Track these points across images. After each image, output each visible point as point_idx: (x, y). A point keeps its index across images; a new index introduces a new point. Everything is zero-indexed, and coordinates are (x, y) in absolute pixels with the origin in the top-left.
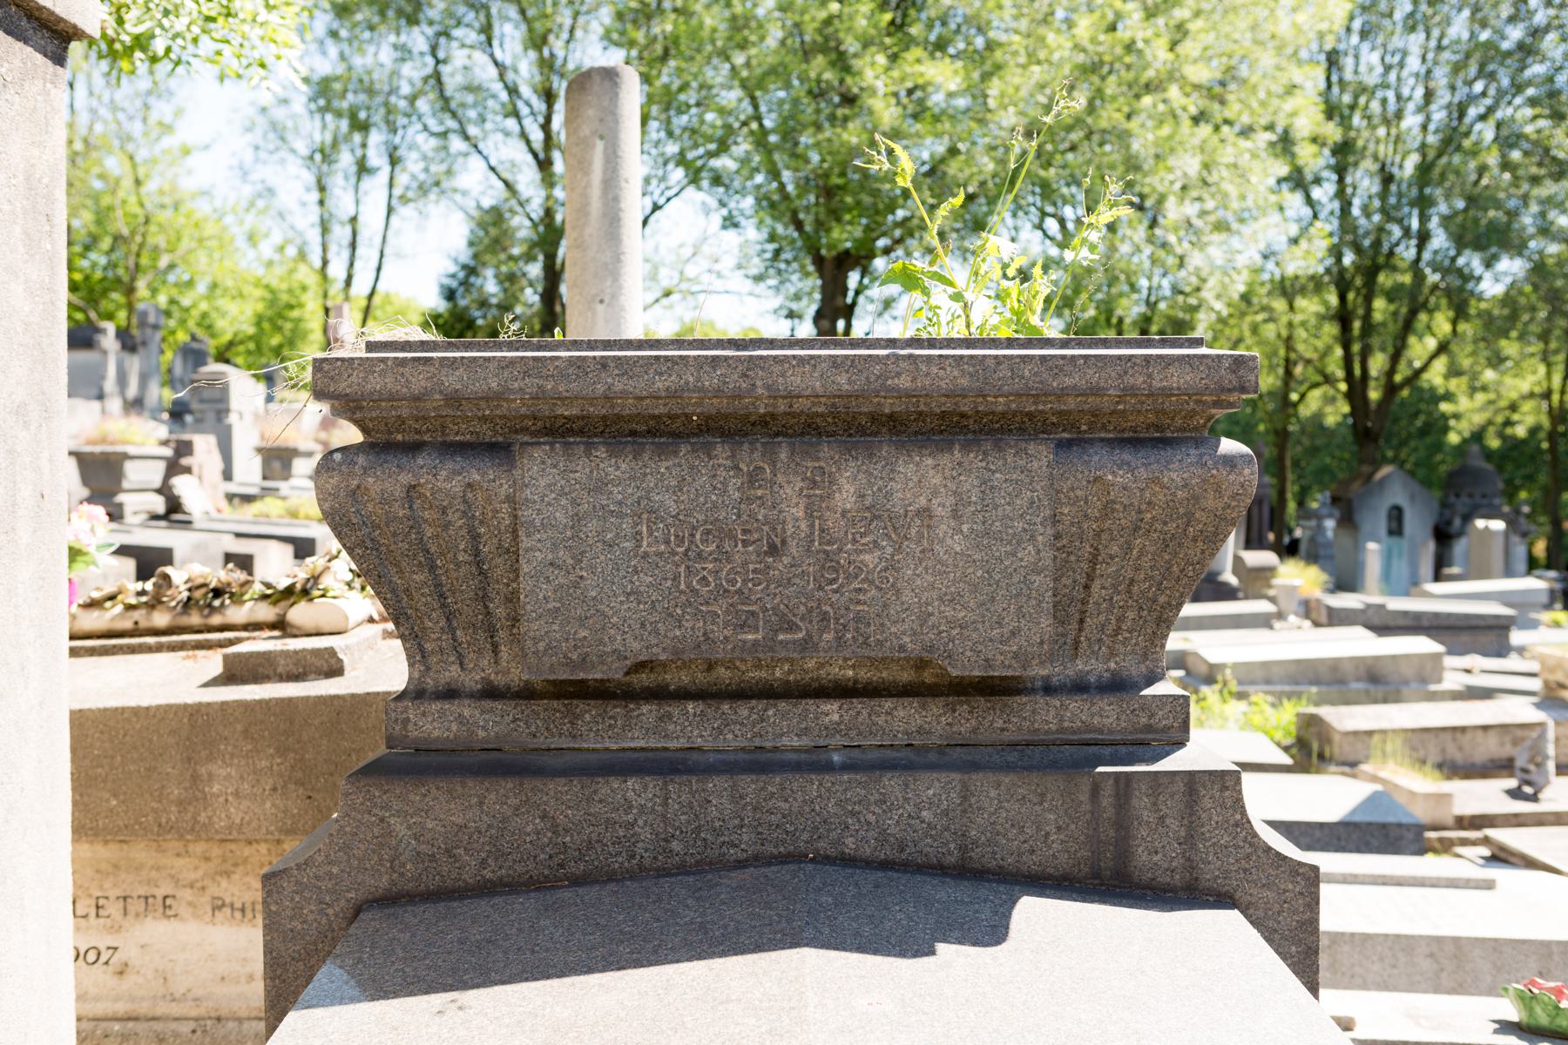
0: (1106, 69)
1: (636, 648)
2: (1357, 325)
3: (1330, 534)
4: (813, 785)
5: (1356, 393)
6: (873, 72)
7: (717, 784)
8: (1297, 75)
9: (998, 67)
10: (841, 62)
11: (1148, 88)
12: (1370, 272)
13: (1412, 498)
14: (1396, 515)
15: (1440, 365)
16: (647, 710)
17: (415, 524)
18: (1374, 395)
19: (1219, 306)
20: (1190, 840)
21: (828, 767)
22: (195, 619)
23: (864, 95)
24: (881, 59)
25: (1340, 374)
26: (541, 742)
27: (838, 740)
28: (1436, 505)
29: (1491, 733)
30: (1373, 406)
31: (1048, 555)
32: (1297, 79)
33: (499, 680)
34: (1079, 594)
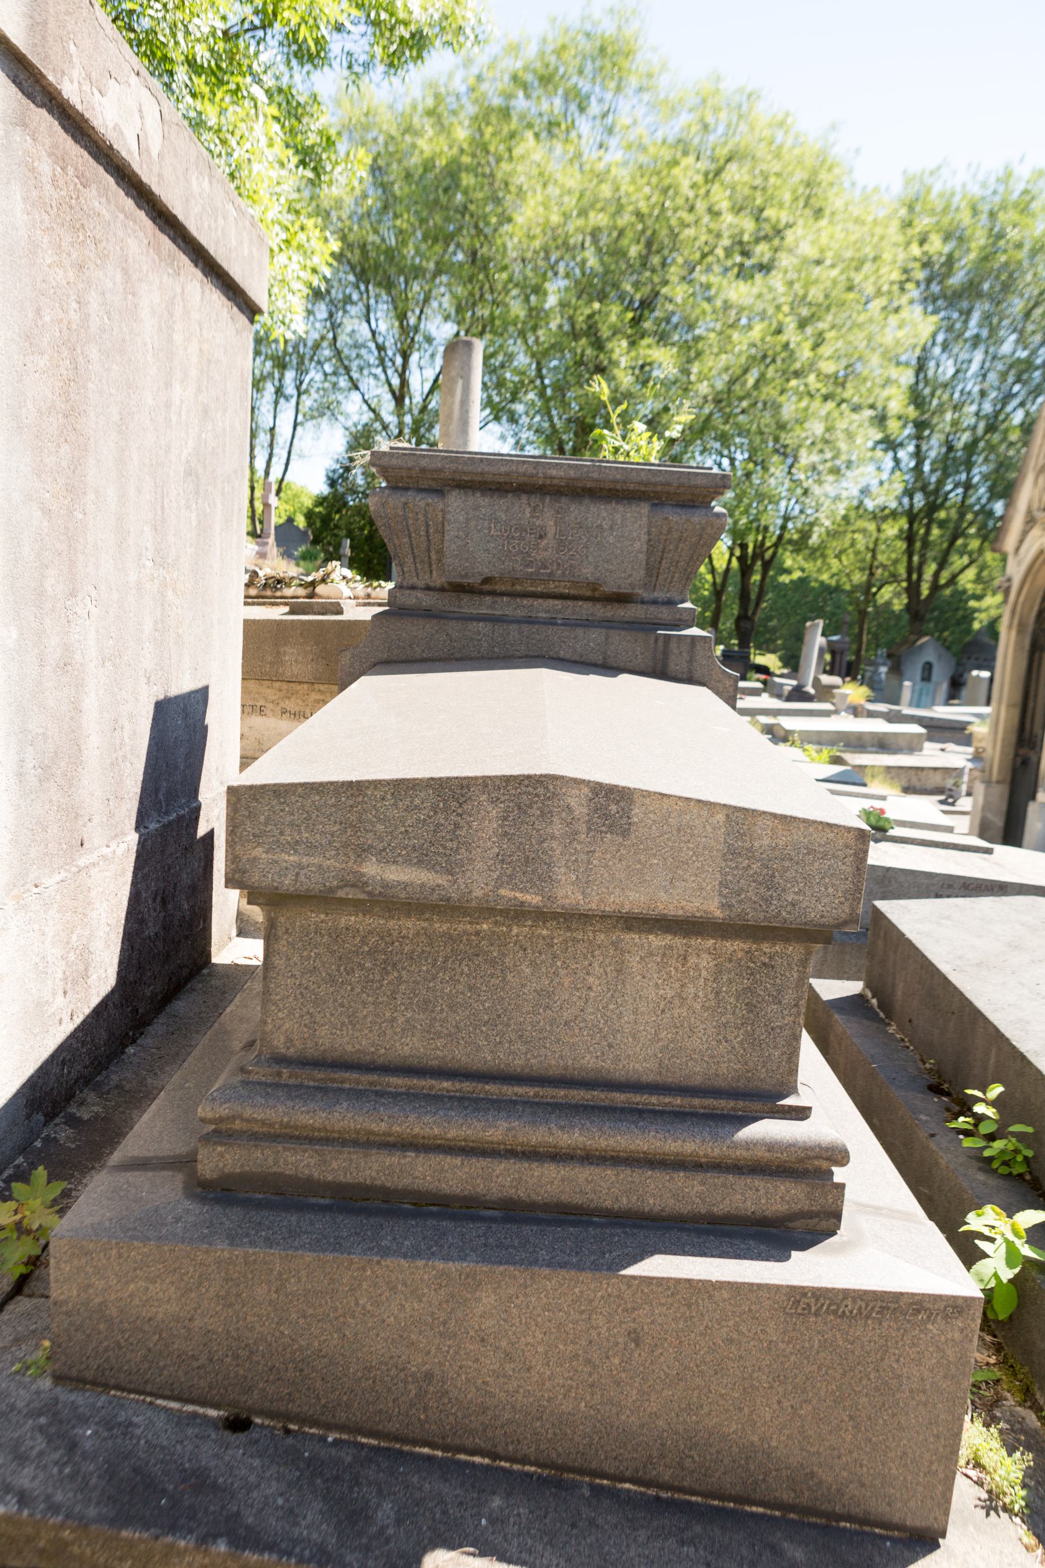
0: (768, 360)
1: (487, 572)
2: (918, 545)
3: (883, 676)
4: (550, 630)
5: (913, 589)
6: (619, 349)
7: (514, 626)
8: (894, 372)
9: (699, 354)
10: (599, 345)
11: (797, 374)
12: (932, 508)
13: (939, 657)
14: (928, 668)
15: (971, 573)
16: (488, 599)
17: (406, 518)
18: (925, 591)
19: (827, 523)
20: (691, 661)
21: (556, 624)
22: (269, 593)
23: (611, 367)
24: (624, 343)
25: (904, 576)
26: (447, 608)
27: (560, 616)
28: (953, 662)
29: (938, 772)
30: (923, 597)
31: (645, 547)
32: (894, 376)
33: (432, 584)
34: (657, 565)
